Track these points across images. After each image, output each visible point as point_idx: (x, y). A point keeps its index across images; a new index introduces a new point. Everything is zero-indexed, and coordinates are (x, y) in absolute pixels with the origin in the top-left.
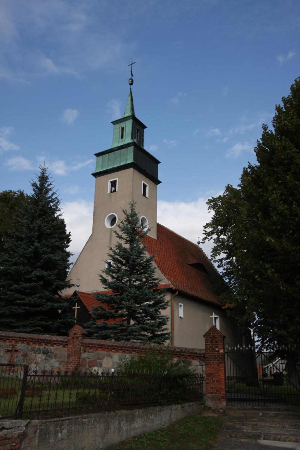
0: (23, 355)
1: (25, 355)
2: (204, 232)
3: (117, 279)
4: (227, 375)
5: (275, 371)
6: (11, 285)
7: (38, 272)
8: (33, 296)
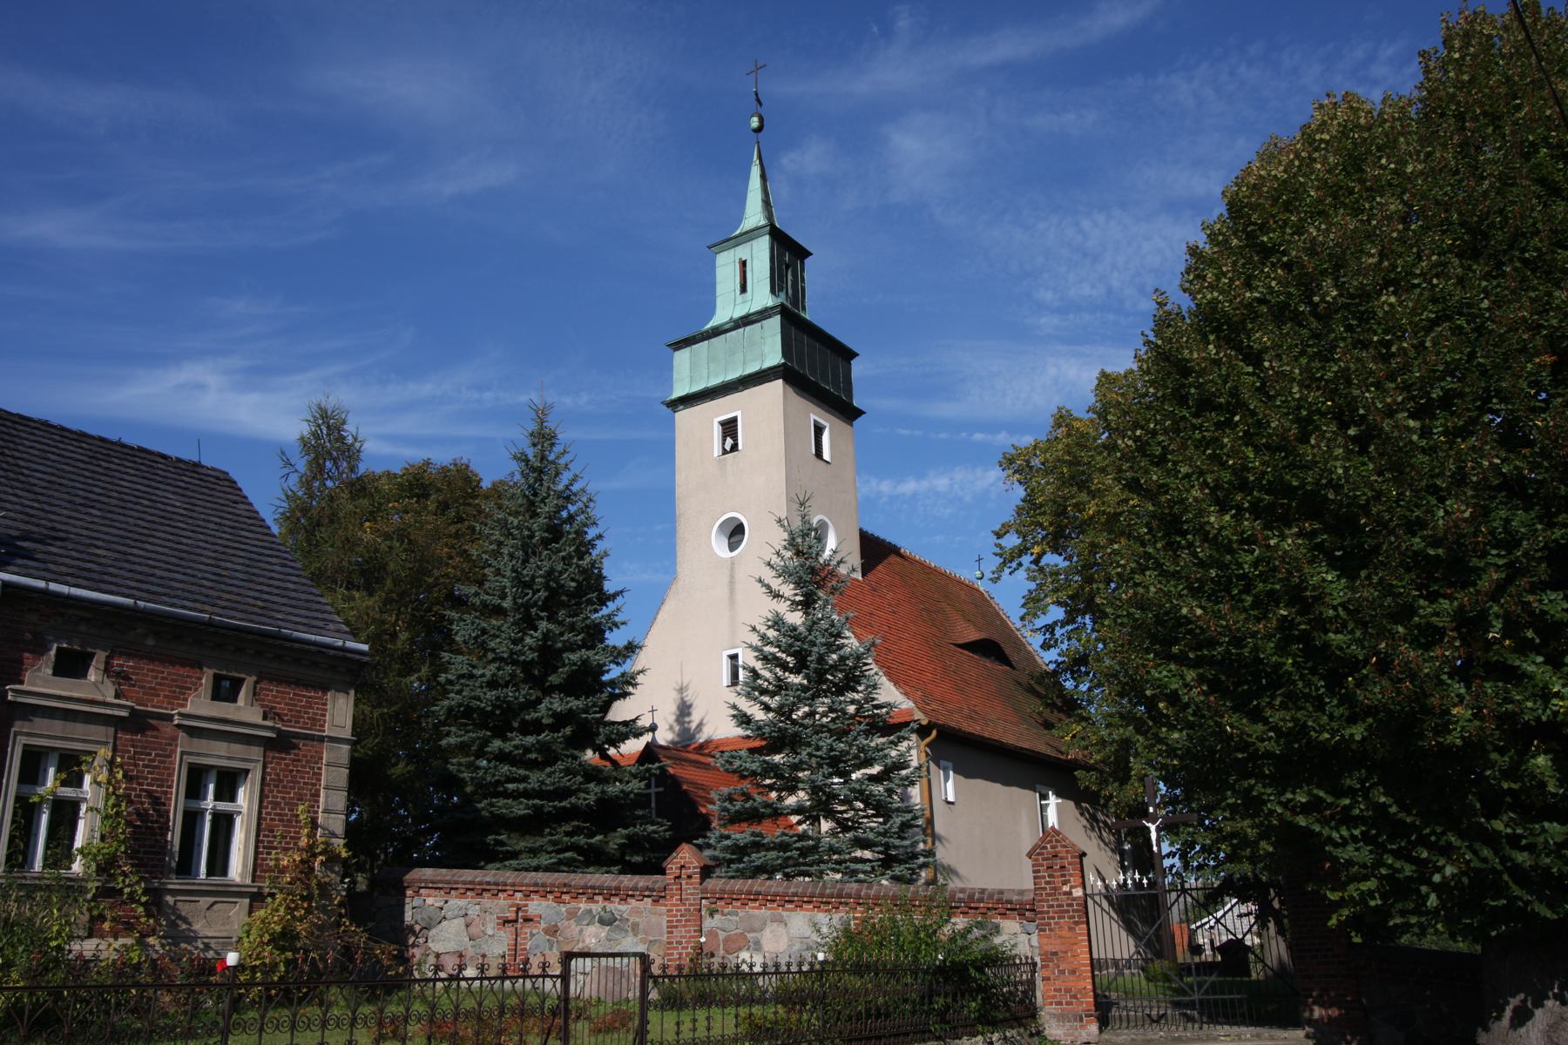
0: (546, 931)
1: (553, 931)
2: (998, 550)
3: (779, 711)
4: (1095, 956)
5: (1224, 939)
6: (486, 742)
7: (556, 703)
8: (548, 770)
